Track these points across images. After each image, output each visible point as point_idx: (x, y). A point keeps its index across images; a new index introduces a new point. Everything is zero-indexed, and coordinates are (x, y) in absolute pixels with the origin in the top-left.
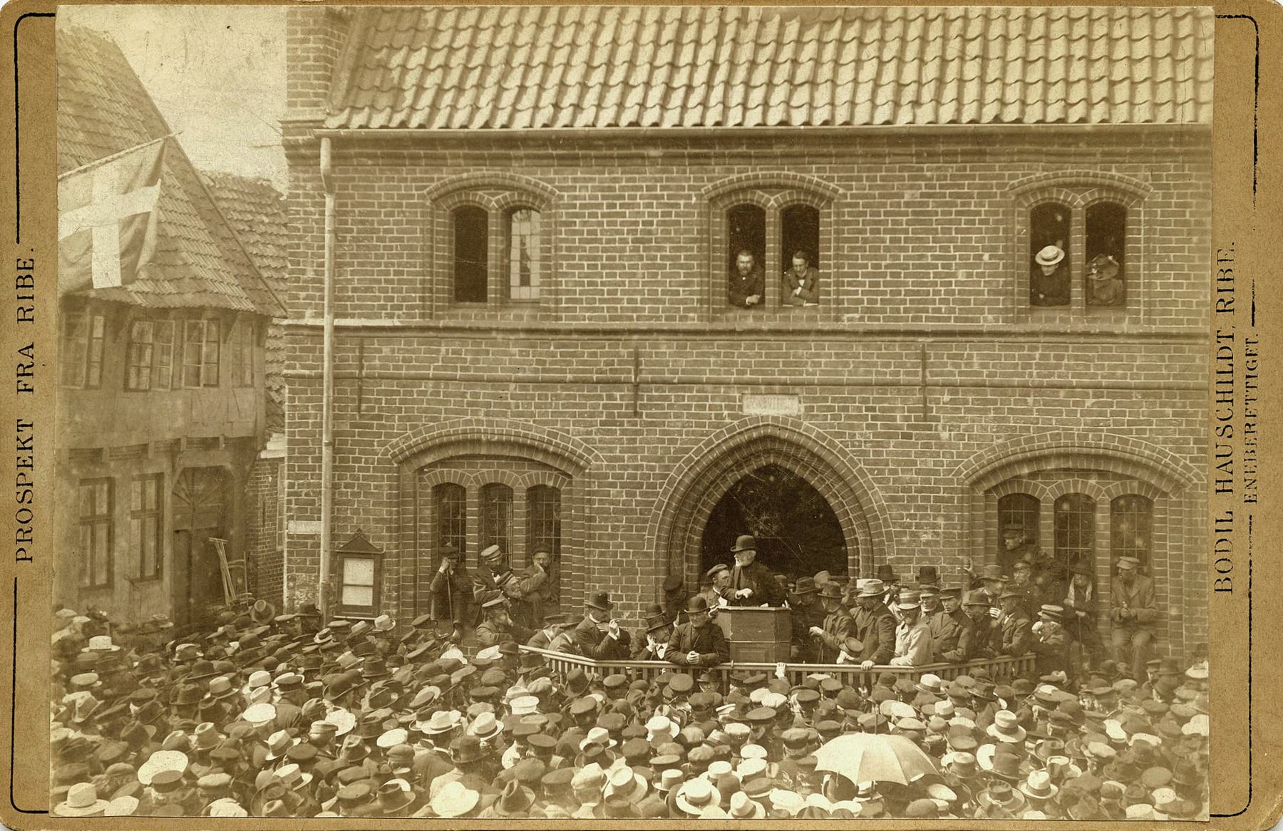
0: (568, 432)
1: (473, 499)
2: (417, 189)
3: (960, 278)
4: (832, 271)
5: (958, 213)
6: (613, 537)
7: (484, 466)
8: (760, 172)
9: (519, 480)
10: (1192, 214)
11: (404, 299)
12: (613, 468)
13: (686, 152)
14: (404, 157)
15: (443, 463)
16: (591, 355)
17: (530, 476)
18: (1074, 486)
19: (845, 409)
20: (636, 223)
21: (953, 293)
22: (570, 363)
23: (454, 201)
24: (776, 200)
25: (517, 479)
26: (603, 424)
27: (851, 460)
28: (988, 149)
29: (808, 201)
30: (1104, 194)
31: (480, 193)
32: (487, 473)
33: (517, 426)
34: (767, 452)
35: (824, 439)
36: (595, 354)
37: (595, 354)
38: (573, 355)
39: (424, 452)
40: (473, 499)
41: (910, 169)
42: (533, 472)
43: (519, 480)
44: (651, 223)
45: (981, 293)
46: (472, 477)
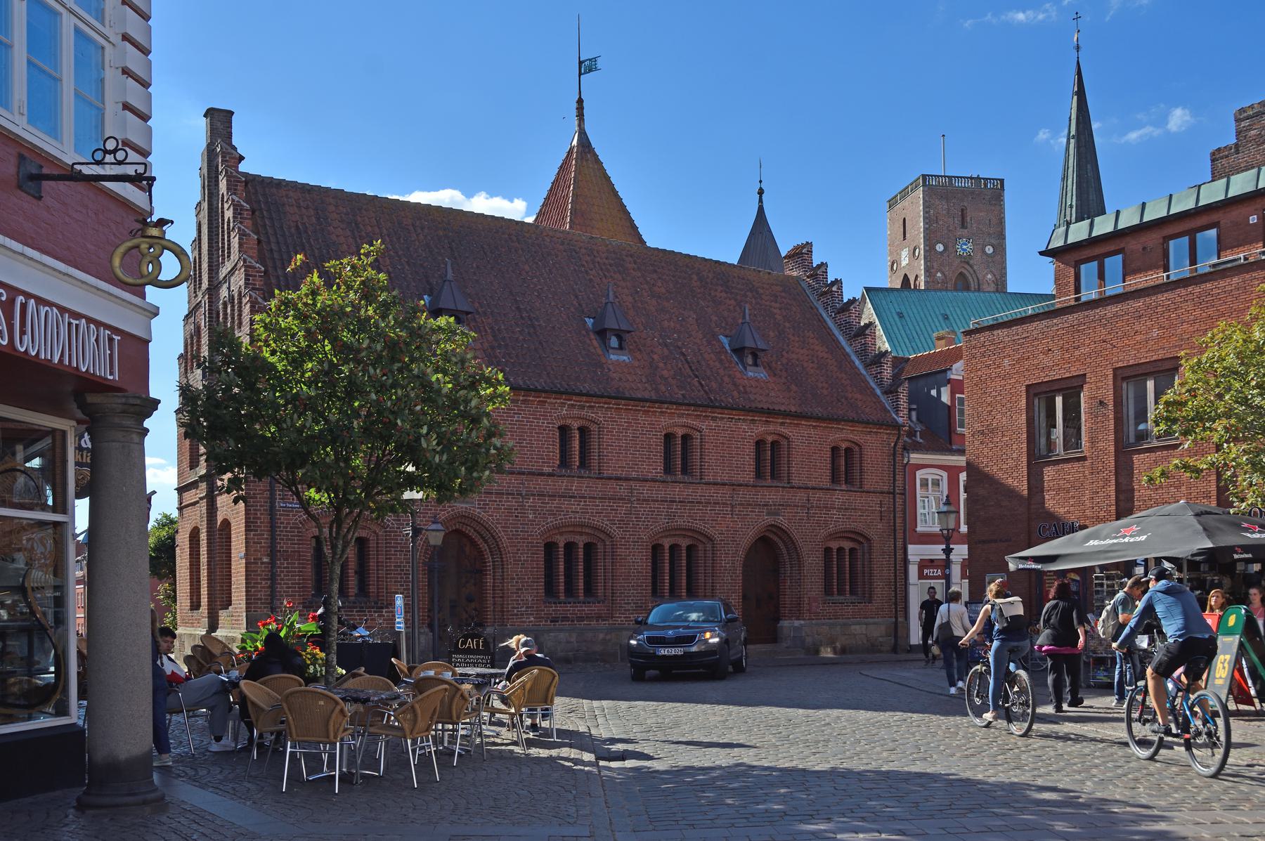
9: (847, 545)
18: (571, 538)
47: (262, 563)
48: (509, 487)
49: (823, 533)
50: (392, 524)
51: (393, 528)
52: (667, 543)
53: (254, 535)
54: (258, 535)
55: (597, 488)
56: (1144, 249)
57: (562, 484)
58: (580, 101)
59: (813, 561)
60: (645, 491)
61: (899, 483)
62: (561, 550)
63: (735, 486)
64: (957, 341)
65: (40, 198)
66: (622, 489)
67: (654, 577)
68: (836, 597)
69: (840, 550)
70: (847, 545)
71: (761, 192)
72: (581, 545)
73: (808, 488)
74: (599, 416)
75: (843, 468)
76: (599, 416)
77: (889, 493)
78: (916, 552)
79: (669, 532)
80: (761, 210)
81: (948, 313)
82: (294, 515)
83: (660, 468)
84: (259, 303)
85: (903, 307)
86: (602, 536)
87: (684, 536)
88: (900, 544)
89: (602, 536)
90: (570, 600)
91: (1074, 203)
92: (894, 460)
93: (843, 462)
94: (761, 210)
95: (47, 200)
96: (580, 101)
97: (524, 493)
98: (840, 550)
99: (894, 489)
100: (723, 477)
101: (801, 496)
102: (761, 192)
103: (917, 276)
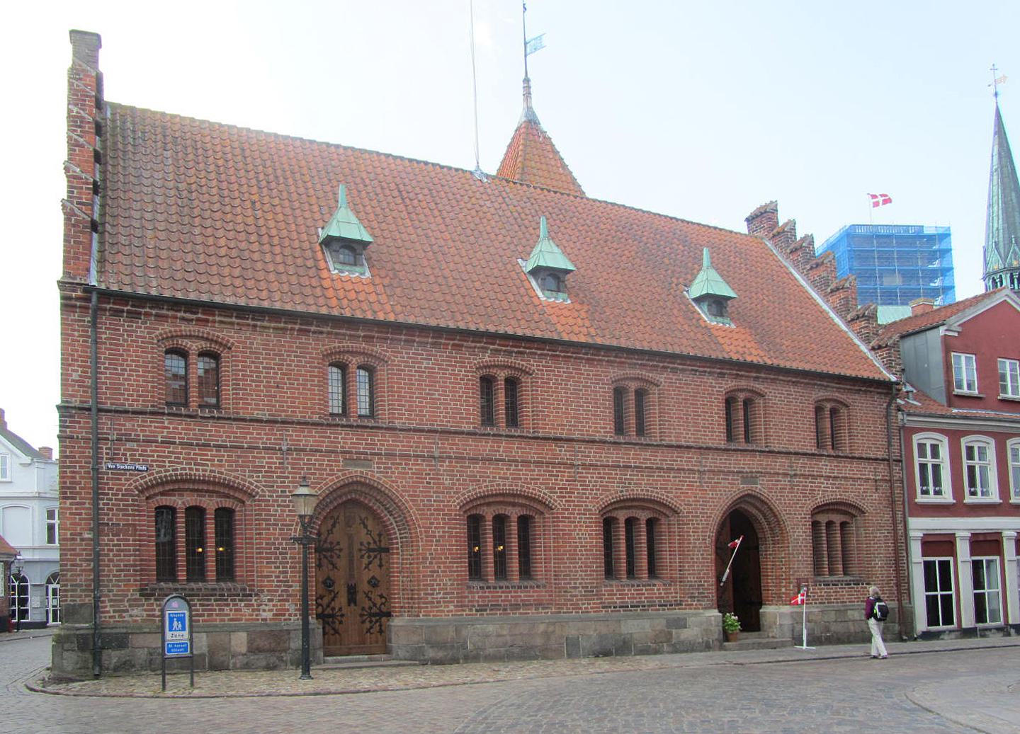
0: (245, 476)
1: (210, 515)
2: (148, 333)
3: (74, 378)
4: (530, 410)
5: (416, 371)
6: (800, 546)
7: (188, 496)
8: (186, 329)
9: (210, 504)
10: (553, 384)
11: (140, 396)
12: (273, 496)
13: (325, 330)
14: (177, 318)
15: (163, 494)
16: (258, 434)
17: (217, 503)
18: (501, 510)
19: (397, 469)
20: (282, 365)
21: (449, 413)
22: (246, 438)
23: (482, 372)
24: (357, 360)
25: (208, 504)
26: (266, 472)
27: (401, 495)
28: (211, 318)
29: (517, 374)
30: (213, 346)
31: (186, 341)
32: (191, 500)
33: (214, 472)
34: (350, 492)
35: (387, 483)
36: (259, 434)
37: (259, 434)
38: (248, 433)
39: (153, 486)
40: (210, 515)
41: (719, 383)
42: (219, 499)
43: (210, 504)
44: (291, 365)
45: (462, 414)
46: (180, 502)
47: (82, 540)
48: (418, 447)
50: (263, 491)
51: (264, 496)
53: (71, 504)
54: (77, 504)
55: (531, 449)
58: (527, 80)
74: (224, 334)
76: (224, 334)
82: (127, 480)
84: (76, 215)
96: (527, 80)
97: (284, 448)
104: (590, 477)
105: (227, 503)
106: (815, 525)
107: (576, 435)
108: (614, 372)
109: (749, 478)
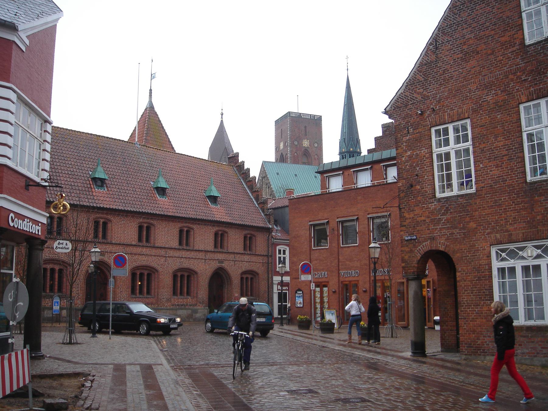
9: (57, 268)
18: (142, 271)
43: (57, 268)
49: (240, 271)
52: (179, 274)
56: (348, 174)
57: (139, 250)
59: (236, 281)
60: (171, 253)
61: (270, 252)
62: (138, 276)
63: (206, 252)
64: (294, 193)
65: (28, 190)
66: (163, 252)
67: (30, 108)
68: (179, 297)
69: (53, 270)
70: (250, 276)
71: (222, 114)
72: (146, 274)
73: (235, 253)
75: (248, 245)
77: (266, 255)
78: (277, 279)
79: (138, 268)
80: (222, 122)
81: (297, 174)
83: (177, 243)
85: (277, 177)
86: (154, 271)
87: (146, 269)
88: (270, 276)
89: (154, 271)
90: (141, 296)
91: (346, 132)
92: (268, 242)
93: (248, 243)
94: (222, 122)
95: (30, 191)
96: (151, 90)
98: (247, 278)
99: (268, 254)
100: (202, 248)
101: (231, 257)
102: (222, 114)
103: (286, 154)
104: (170, 260)
105: (62, 267)
106: (242, 278)
107: (167, 246)
108: (180, 225)
109: (221, 262)
